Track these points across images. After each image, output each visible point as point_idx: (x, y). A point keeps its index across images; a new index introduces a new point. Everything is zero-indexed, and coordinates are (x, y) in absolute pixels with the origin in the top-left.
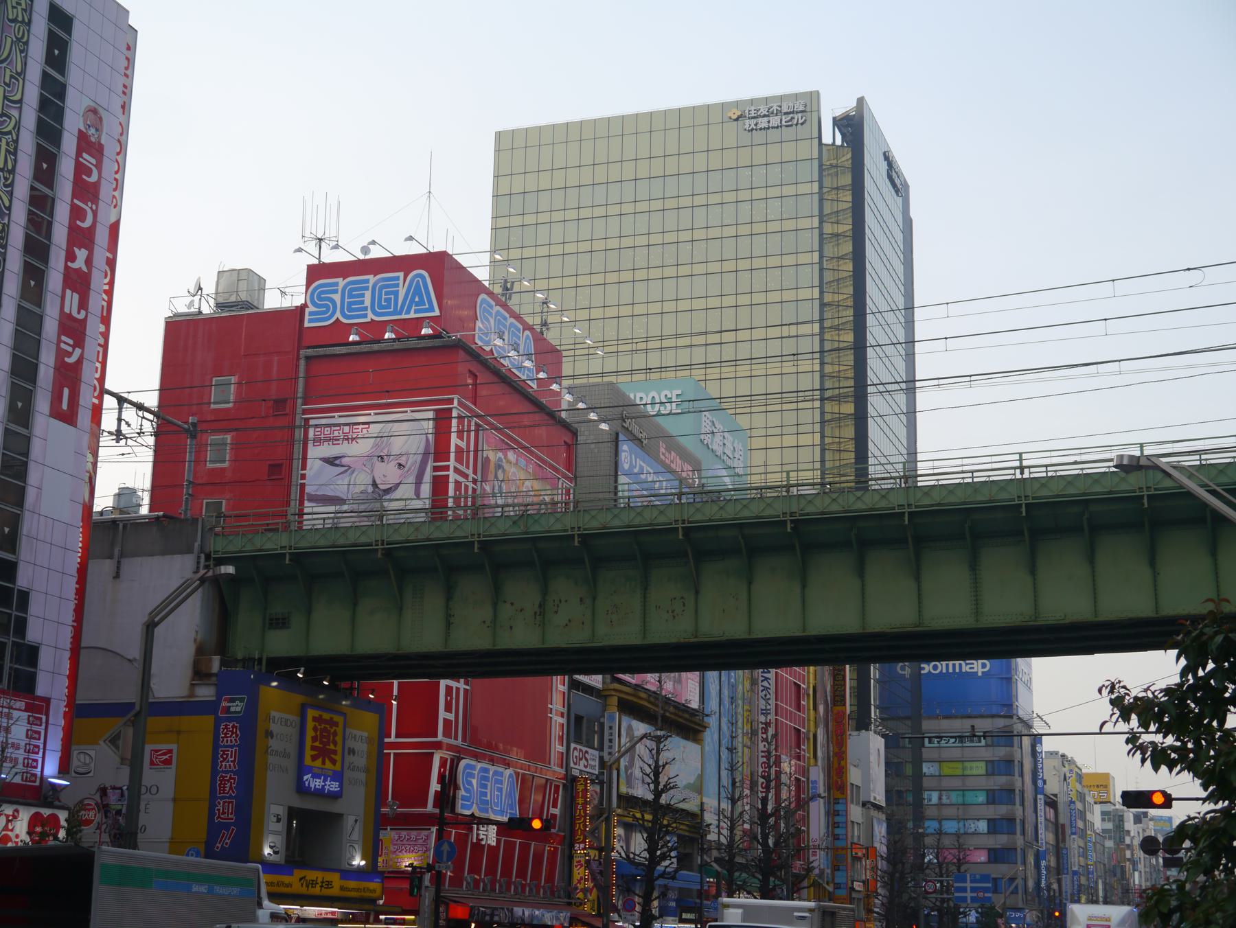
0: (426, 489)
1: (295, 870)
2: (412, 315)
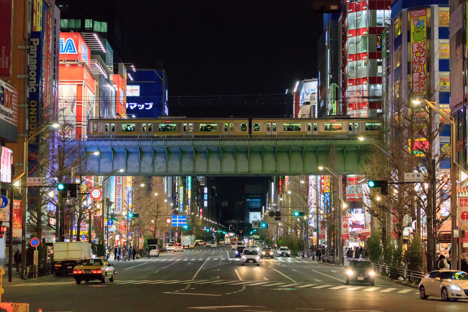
0: (75, 109)
2: (68, 53)
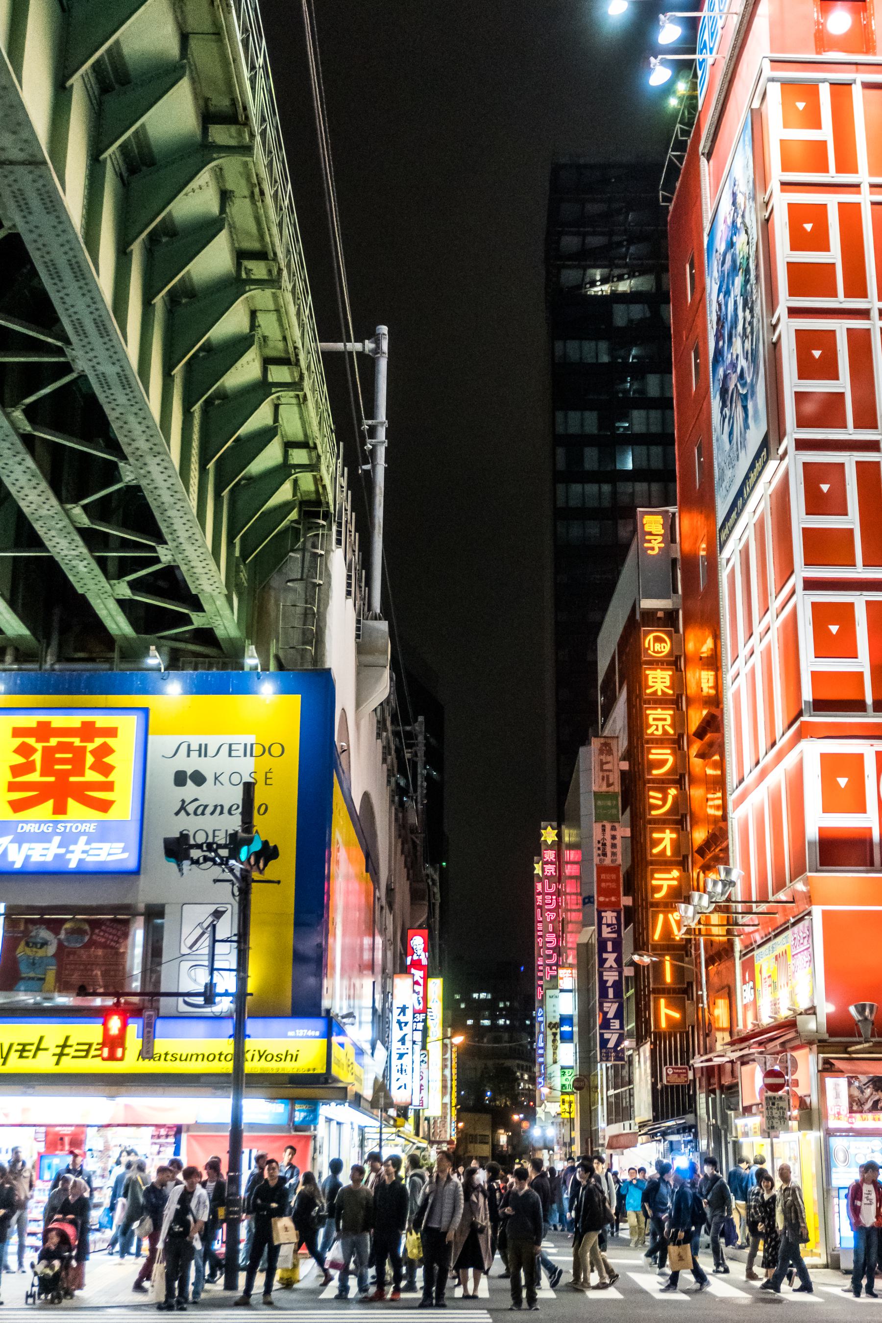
1: (298, 697)
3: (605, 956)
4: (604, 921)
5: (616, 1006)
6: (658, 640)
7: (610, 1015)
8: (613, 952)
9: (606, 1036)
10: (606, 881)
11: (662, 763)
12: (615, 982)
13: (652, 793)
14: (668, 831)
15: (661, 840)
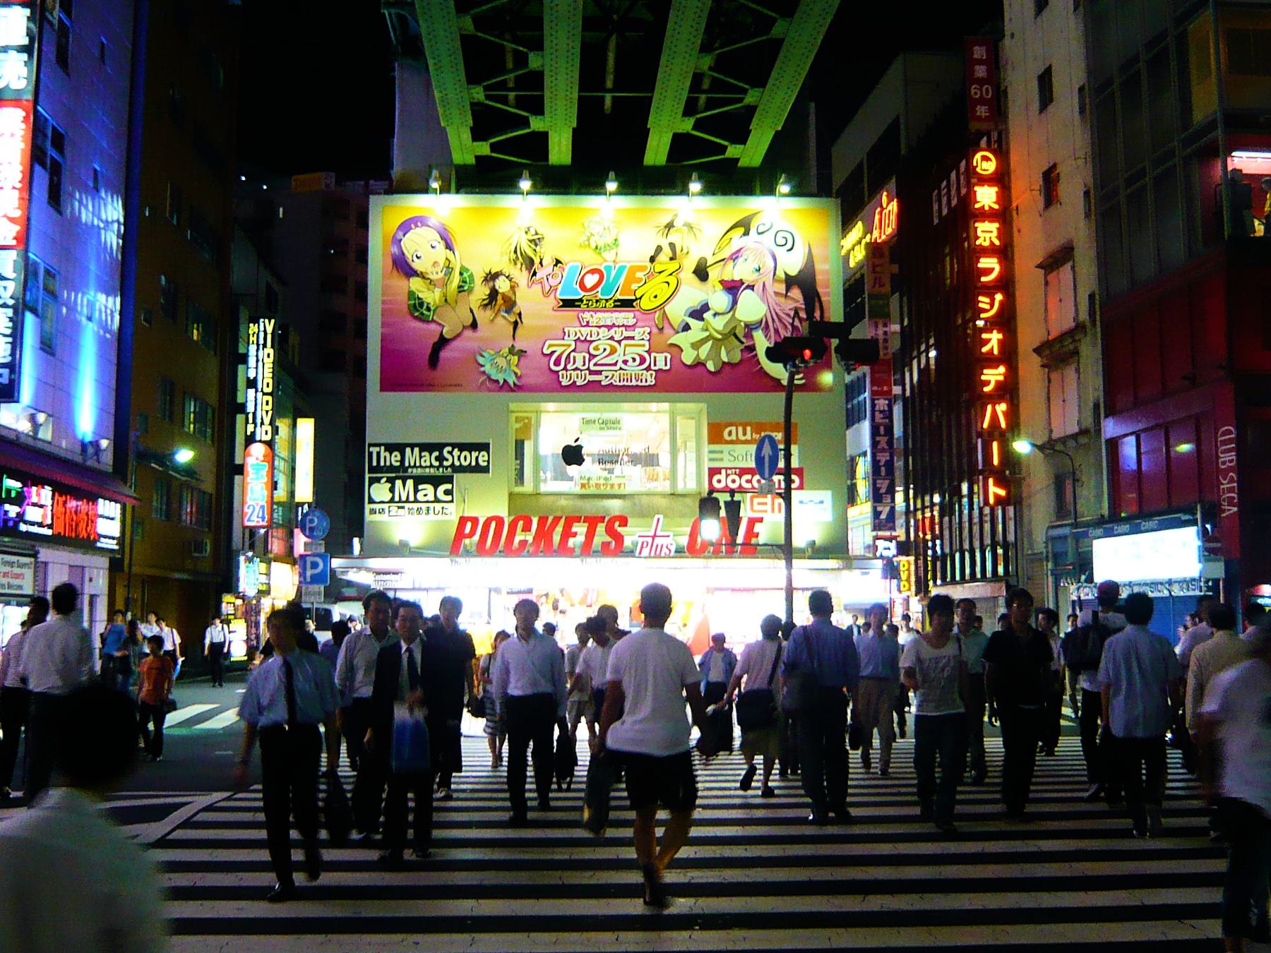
3: (878, 439)
4: (877, 408)
5: (887, 482)
6: (985, 158)
7: (883, 491)
8: (885, 435)
9: (879, 509)
10: (879, 372)
11: (989, 271)
12: (887, 461)
13: (981, 298)
14: (995, 332)
15: (988, 341)
